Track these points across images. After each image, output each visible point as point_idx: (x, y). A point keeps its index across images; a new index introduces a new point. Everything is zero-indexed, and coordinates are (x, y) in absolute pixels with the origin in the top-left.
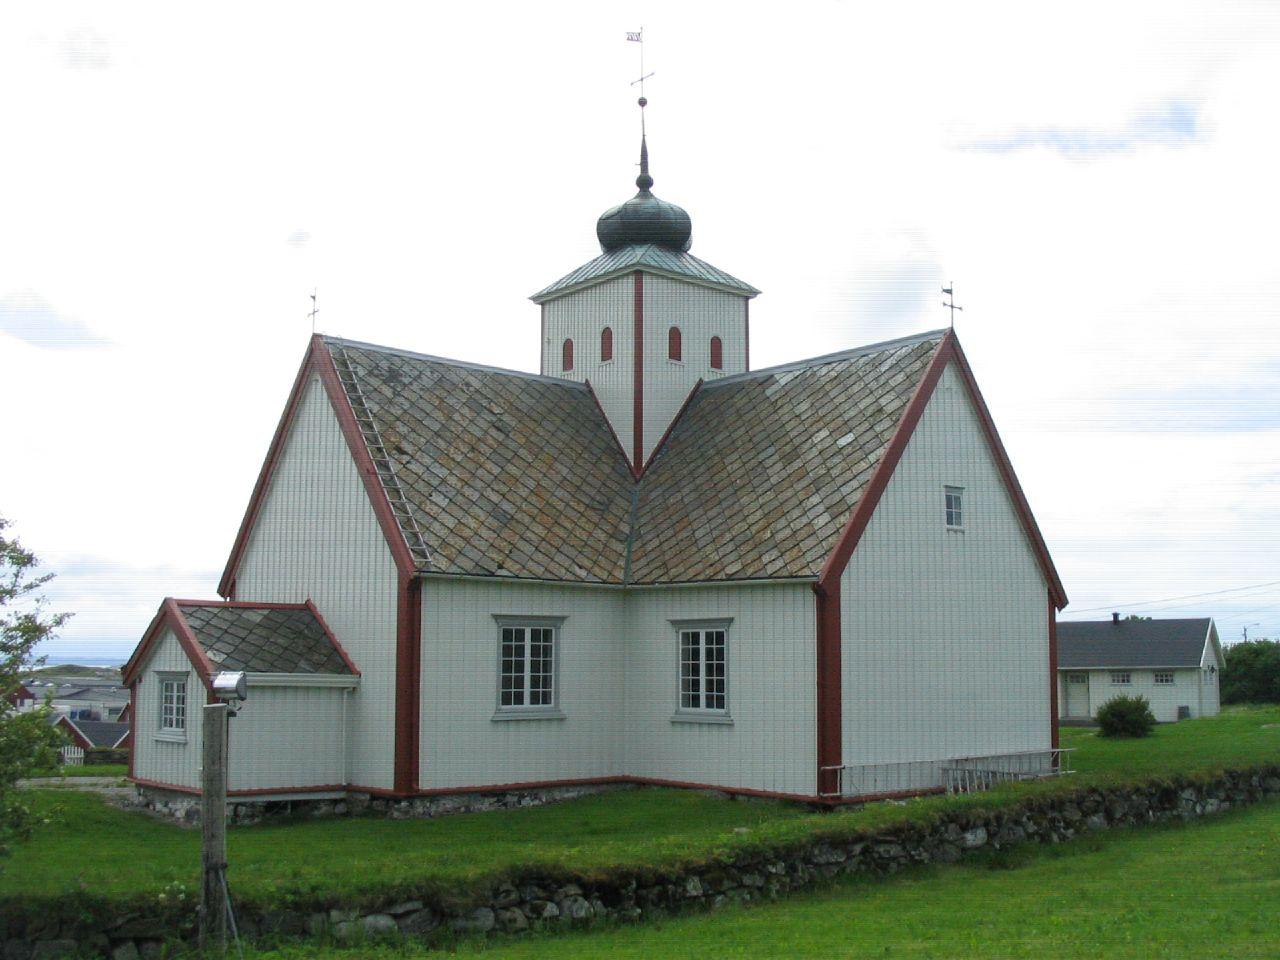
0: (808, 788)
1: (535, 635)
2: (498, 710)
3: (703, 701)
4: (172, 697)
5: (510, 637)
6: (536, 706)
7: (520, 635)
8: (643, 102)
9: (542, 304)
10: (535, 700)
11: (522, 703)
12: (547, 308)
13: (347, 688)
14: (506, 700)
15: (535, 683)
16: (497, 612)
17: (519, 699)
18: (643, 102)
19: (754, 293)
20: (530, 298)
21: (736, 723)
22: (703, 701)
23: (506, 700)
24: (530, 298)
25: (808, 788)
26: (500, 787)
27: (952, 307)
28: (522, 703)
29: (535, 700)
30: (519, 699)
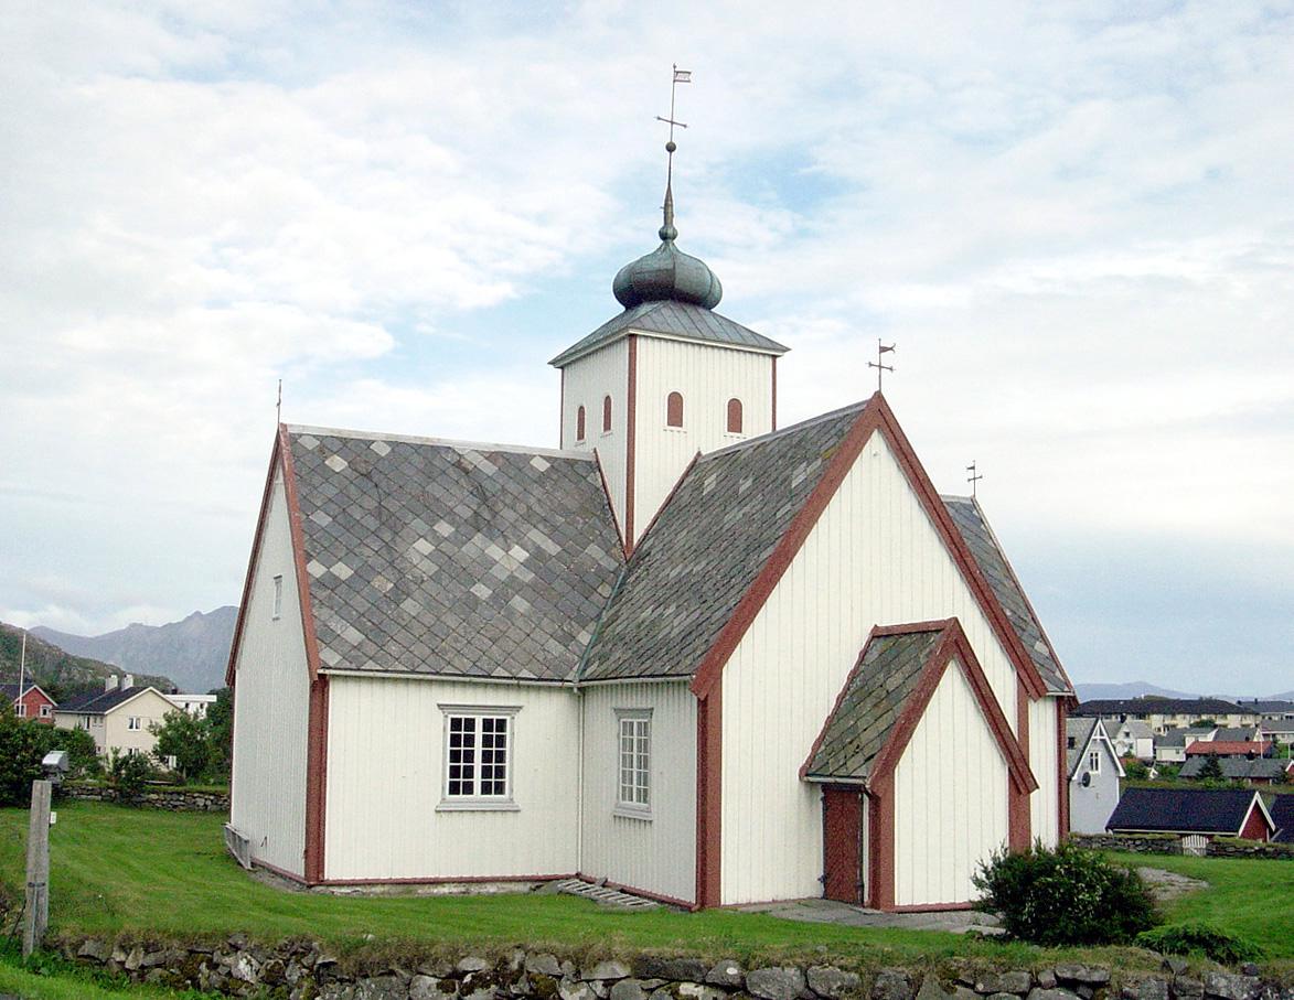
0: (689, 895)
1: (487, 725)
2: (617, 806)
3: (477, 787)
4: (639, 734)
5: (460, 730)
6: (488, 796)
7: (470, 724)
8: (671, 148)
9: (562, 368)
10: (486, 789)
11: (472, 793)
12: (566, 370)
13: (1147, 944)
14: (454, 789)
15: (486, 772)
16: (620, 705)
17: (469, 789)
18: (671, 148)
19: (787, 350)
20: (549, 363)
21: (655, 822)
22: (477, 787)
23: (454, 789)
24: (549, 363)
25: (689, 895)
26: (151, 630)
27: (880, 367)
28: (472, 793)
29: (486, 789)
30: (469, 789)
